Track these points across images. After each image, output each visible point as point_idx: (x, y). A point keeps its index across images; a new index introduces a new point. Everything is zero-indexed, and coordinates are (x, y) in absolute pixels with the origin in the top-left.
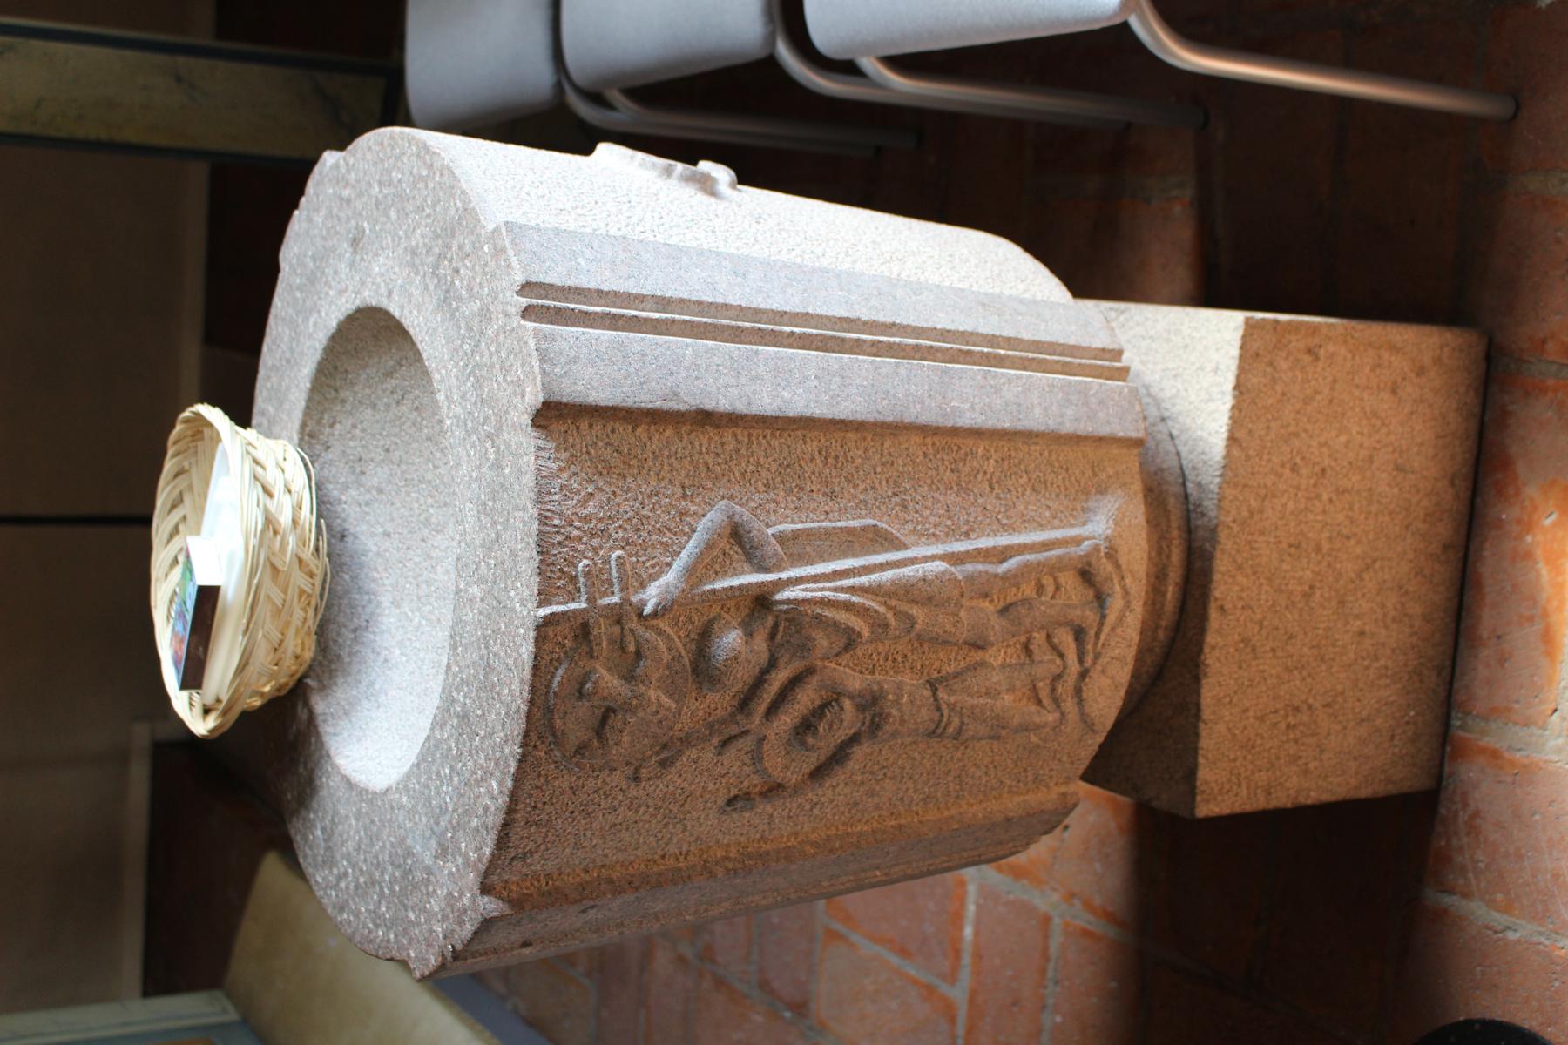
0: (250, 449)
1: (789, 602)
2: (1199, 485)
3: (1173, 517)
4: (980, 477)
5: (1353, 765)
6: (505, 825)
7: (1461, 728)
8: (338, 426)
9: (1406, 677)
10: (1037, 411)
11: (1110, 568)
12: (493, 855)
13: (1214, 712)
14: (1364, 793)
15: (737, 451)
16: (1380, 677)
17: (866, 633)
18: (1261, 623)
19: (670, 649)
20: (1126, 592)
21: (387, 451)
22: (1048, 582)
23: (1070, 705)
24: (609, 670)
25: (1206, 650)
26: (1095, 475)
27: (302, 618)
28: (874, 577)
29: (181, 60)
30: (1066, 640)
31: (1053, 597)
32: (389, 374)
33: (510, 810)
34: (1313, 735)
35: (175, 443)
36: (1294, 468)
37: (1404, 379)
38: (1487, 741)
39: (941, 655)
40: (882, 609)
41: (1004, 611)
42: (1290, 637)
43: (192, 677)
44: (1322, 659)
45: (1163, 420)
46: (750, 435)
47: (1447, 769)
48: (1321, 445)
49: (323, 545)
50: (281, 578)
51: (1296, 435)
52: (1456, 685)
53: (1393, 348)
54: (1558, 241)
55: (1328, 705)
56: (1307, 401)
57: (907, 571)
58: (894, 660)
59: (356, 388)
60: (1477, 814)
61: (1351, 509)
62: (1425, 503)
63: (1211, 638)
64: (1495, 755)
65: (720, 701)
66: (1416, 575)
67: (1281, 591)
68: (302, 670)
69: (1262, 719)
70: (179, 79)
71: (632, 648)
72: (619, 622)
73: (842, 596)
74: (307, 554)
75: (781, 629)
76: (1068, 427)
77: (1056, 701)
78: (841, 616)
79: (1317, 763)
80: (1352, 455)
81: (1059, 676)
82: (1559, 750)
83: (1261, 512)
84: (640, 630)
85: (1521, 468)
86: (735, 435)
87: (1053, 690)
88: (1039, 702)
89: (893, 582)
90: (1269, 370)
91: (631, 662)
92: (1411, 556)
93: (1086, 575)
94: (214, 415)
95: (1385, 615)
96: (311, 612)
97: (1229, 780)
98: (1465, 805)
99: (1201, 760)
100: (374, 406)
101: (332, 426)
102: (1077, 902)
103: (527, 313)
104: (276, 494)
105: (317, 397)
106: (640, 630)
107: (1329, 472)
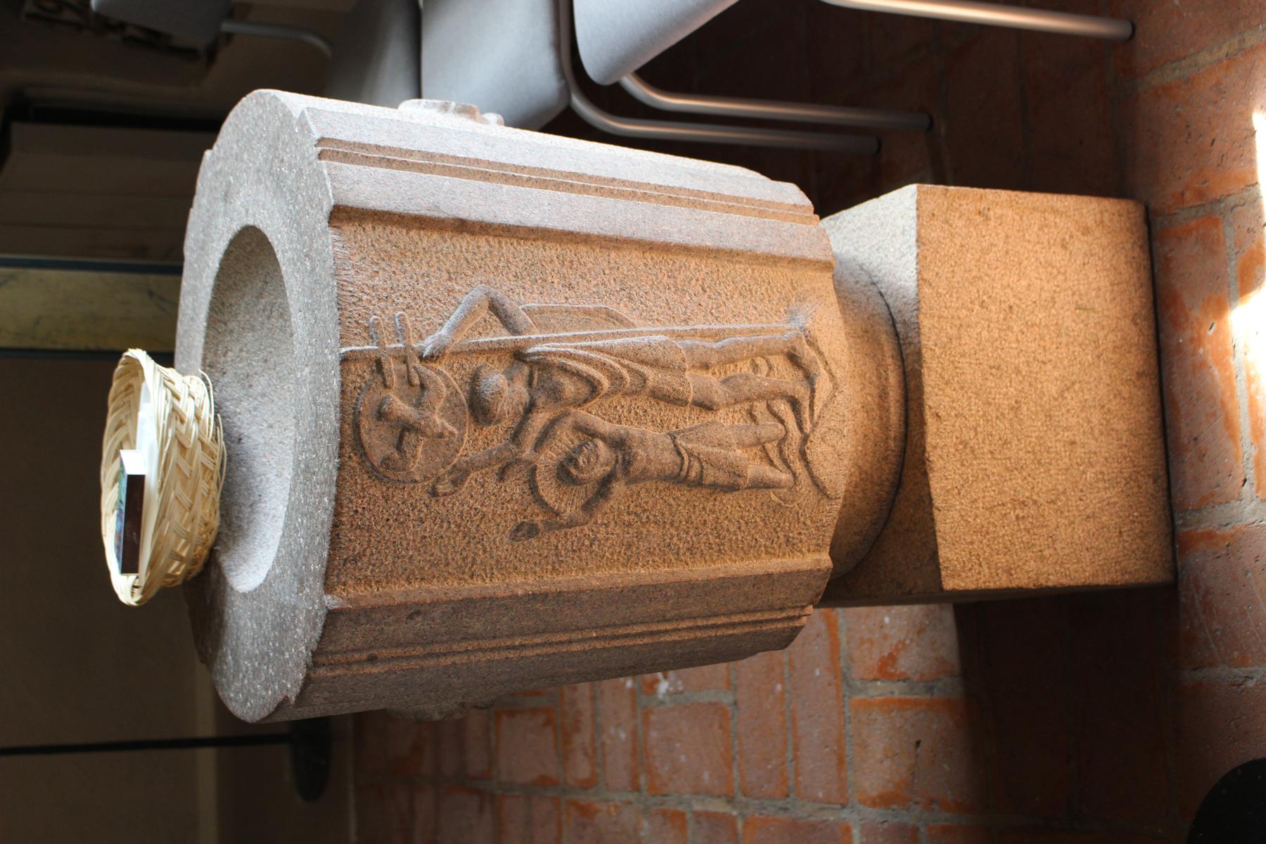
0: (169, 384)
1: (538, 353)
2: (904, 322)
3: (886, 349)
4: (693, 282)
5: (1088, 556)
6: (335, 526)
7: (1184, 525)
8: (230, 354)
9: (1123, 482)
10: (736, 238)
11: (813, 354)
12: (329, 555)
13: (945, 501)
14: (1103, 580)
15: (491, 252)
16: (1098, 481)
17: (606, 384)
18: (975, 430)
19: (448, 386)
20: (832, 376)
21: (266, 361)
22: (759, 361)
23: (798, 466)
24: (401, 398)
25: (929, 448)
26: (794, 289)
27: (208, 489)
28: (609, 341)
29: (152, 278)
30: (783, 408)
31: (768, 375)
32: (260, 296)
33: (337, 513)
34: (1043, 527)
35: (114, 399)
36: (982, 304)
37: (1071, 237)
38: (1204, 527)
39: (677, 413)
40: (617, 365)
41: (725, 382)
42: (1005, 443)
43: (129, 565)
44: (1039, 463)
45: (873, 284)
46: (500, 243)
47: (1179, 564)
48: (1003, 287)
49: (221, 434)
50: (188, 453)
51: (980, 278)
52: (1173, 491)
53: (1055, 211)
54: (1179, 115)
55: (1053, 502)
56: (984, 252)
57: (636, 339)
58: (636, 414)
59: (240, 318)
60: (1207, 592)
61: (1042, 339)
62: (1111, 337)
63: (931, 440)
64: (1210, 535)
65: (495, 436)
66: (1115, 397)
67: (990, 404)
68: (211, 538)
69: (991, 510)
70: (151, 294)
71: (417, 381)
72: (405, 362)
73: (581, 352)
74: (208, 440)
75: (536, 376)
76: (762, 249)
77: (785, 461)
78: (583, 367)
79: (1051, 551)
80: (1034, 296)
81: (784, 439)
82: (1254, 512)
83: (960, 339)
84: (422, 368)
85: (1186, 299)
86: (488, 241)
87: (781, 451)
88: (771, 463)
89: (623, 345)
90: (946, 226)
91: (419, 390)
92: (1106, 379)
93: (793, 358)
94: (139, 354)
95: (1092, 428)
96: (214, 485)
97: (970, 560)
98: (1198, 587)
99: (939, 540)
100: (253, 329)
101: (225, 355)
102: (935, 806)
103: (321, 156)
104: (182, 397)
105: (211, 333)
106: (422, 368)
107: (1015, 308)
